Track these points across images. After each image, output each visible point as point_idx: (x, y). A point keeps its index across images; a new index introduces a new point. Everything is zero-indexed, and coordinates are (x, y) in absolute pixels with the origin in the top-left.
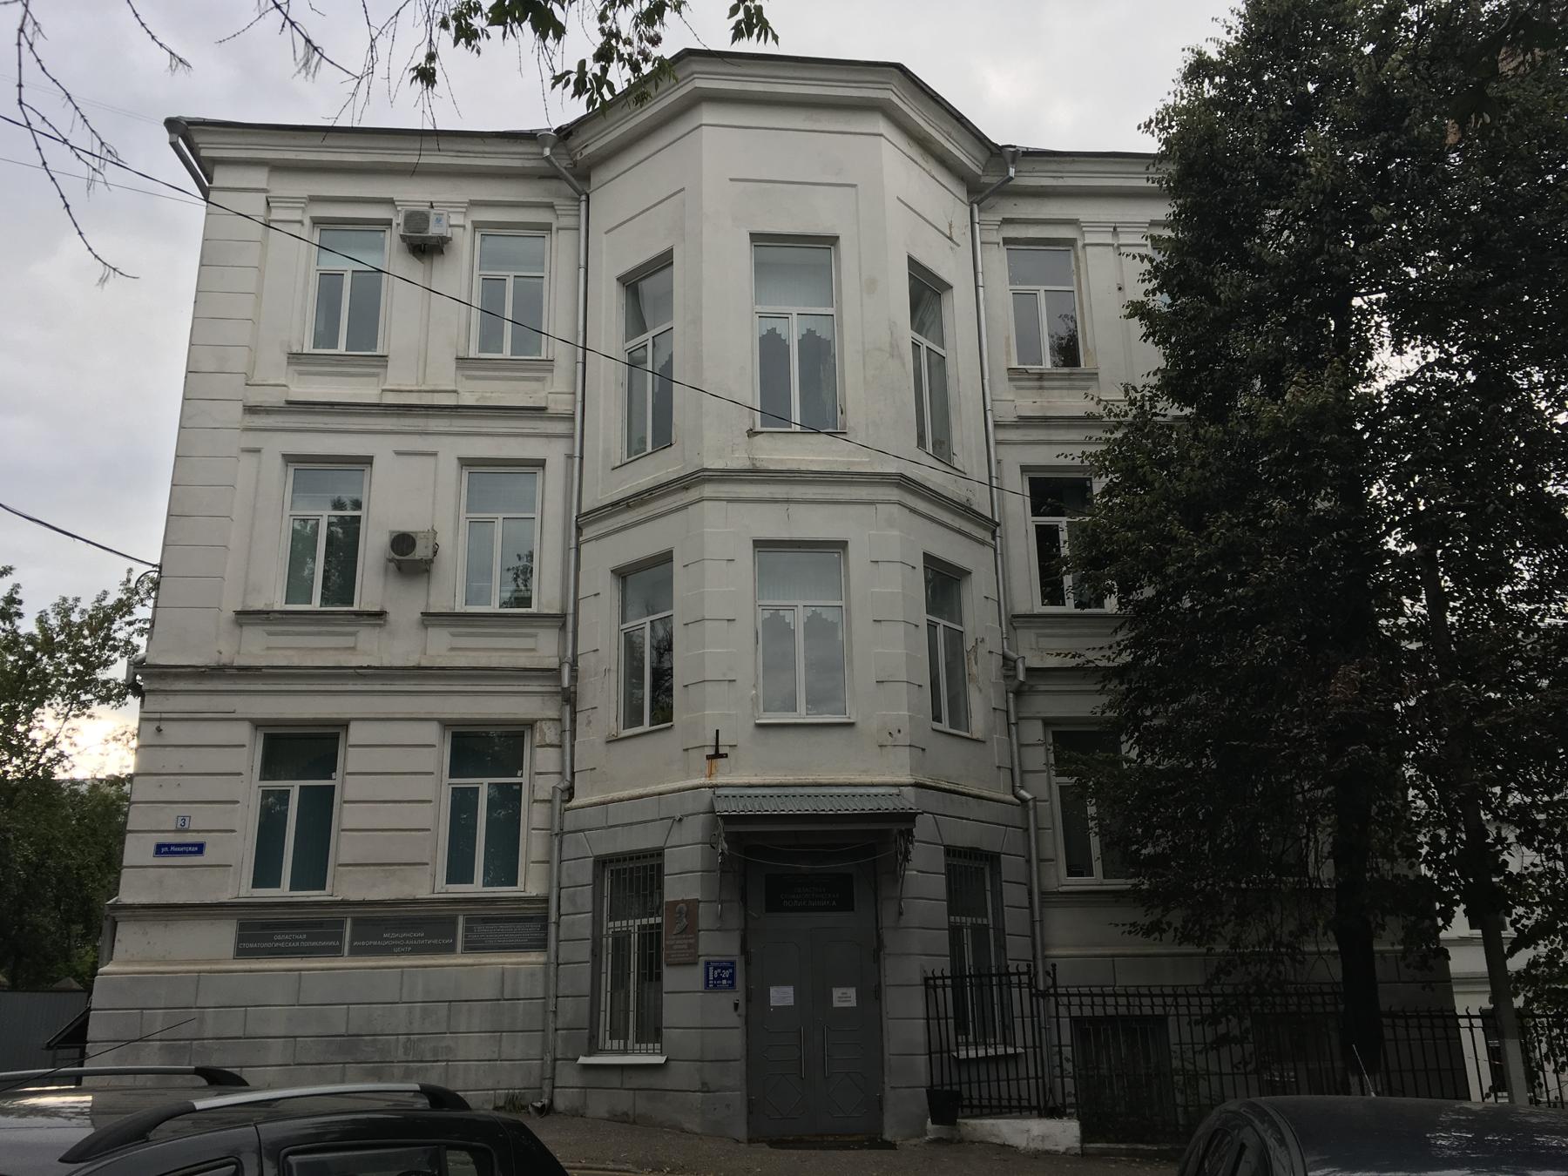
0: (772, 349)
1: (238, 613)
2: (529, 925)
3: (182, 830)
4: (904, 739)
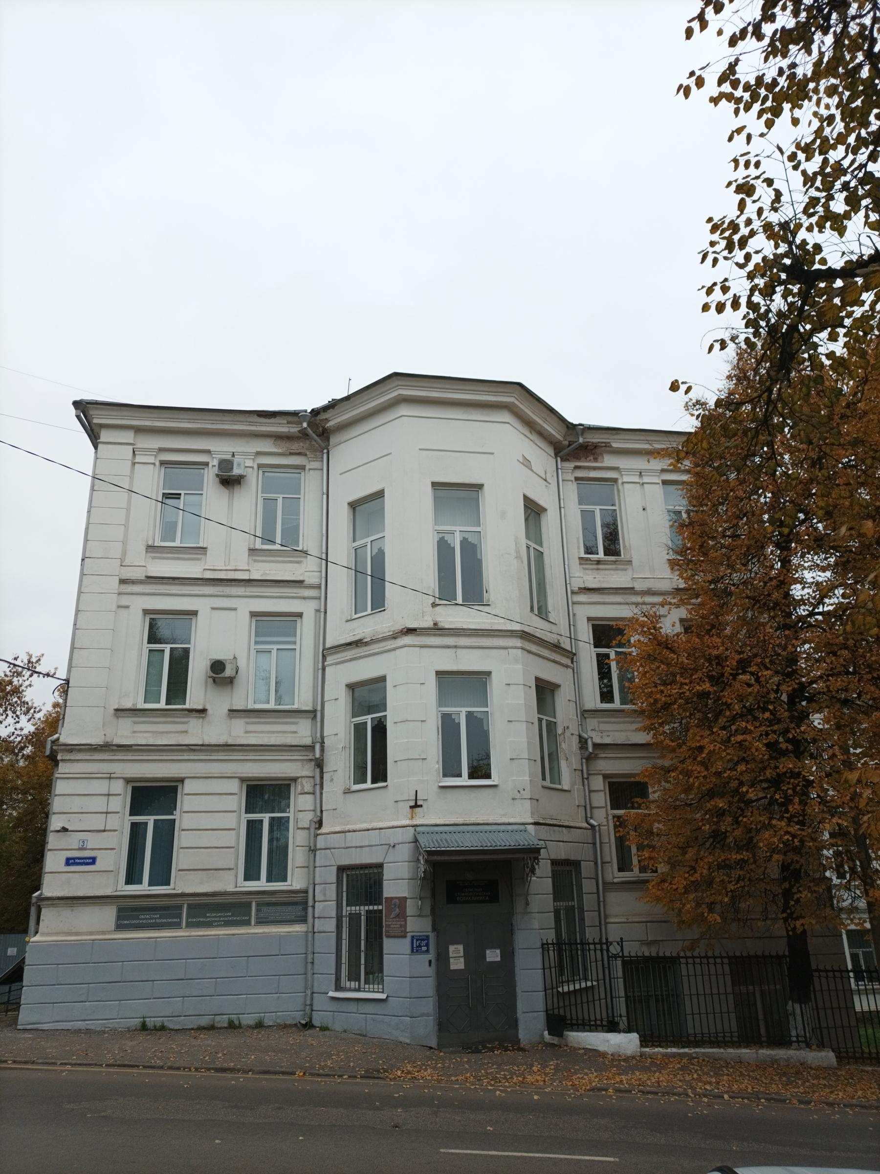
0: (444, 549)
1: (117, 710)
2: (297, 906)
3: (82, 849)
4: (527, 794)
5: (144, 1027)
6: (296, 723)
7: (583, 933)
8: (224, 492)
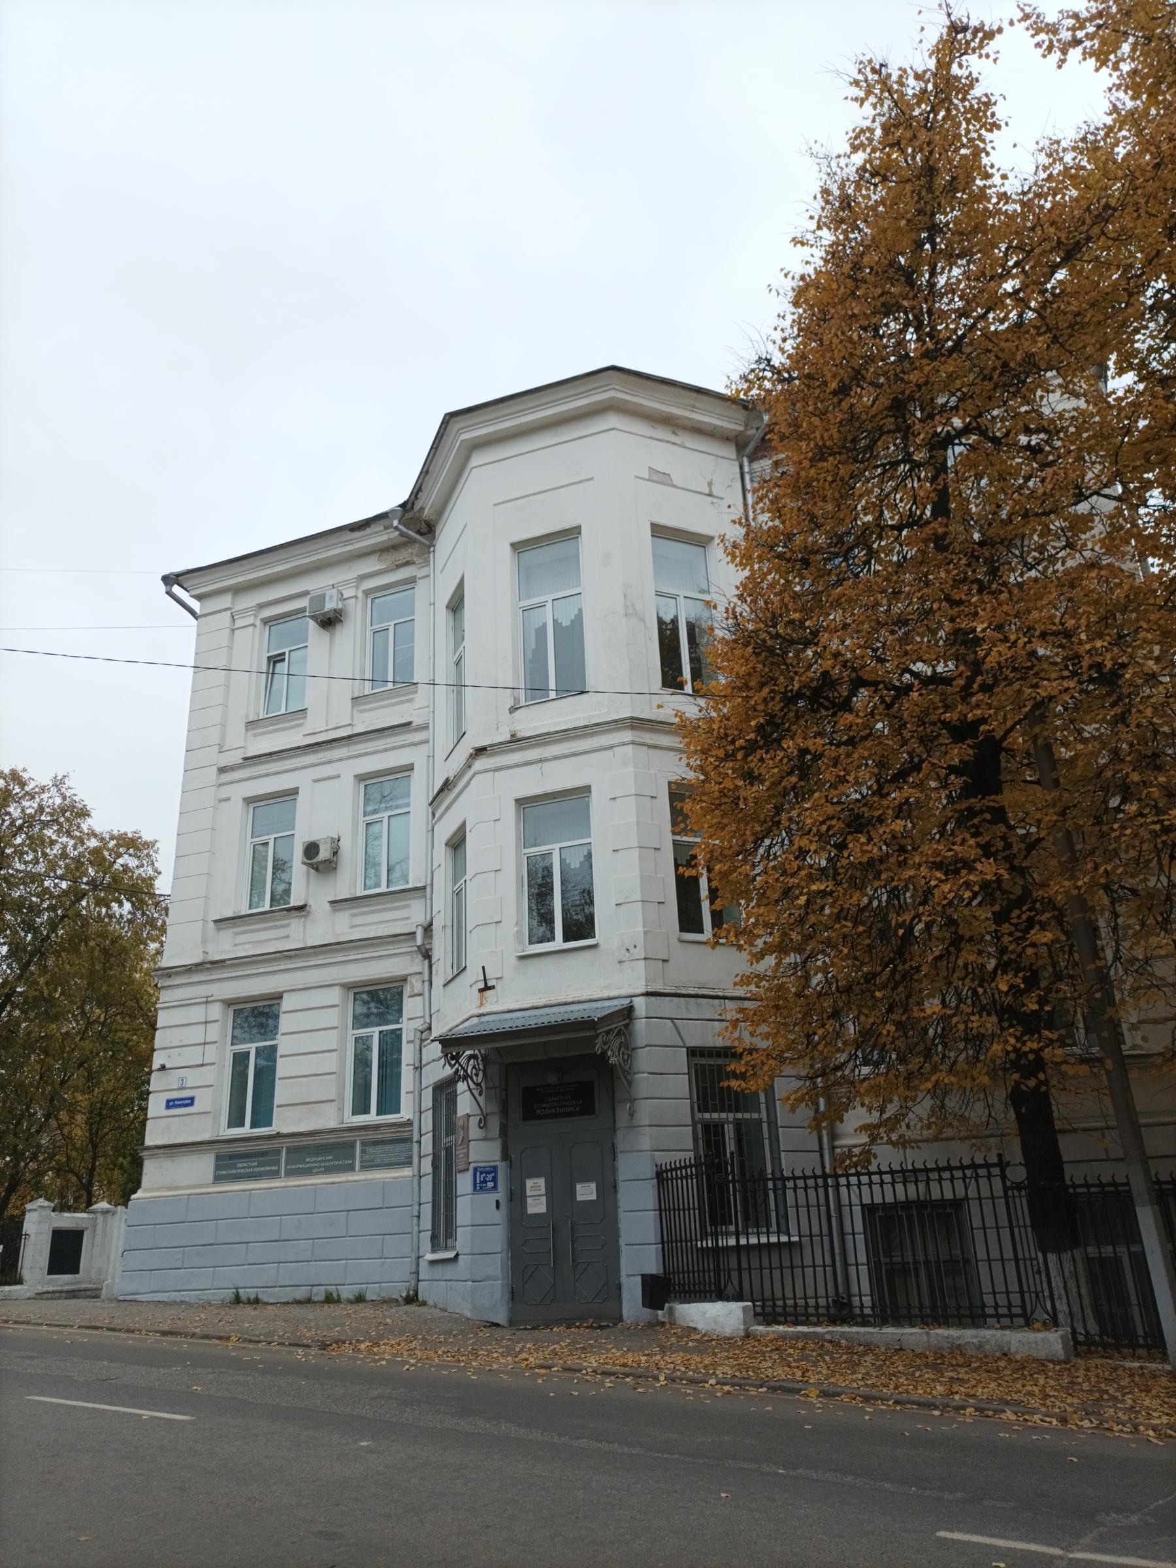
5: (237, 1300)
6: (407, 907)
7: (776, 1159)
8: (325, 635)
